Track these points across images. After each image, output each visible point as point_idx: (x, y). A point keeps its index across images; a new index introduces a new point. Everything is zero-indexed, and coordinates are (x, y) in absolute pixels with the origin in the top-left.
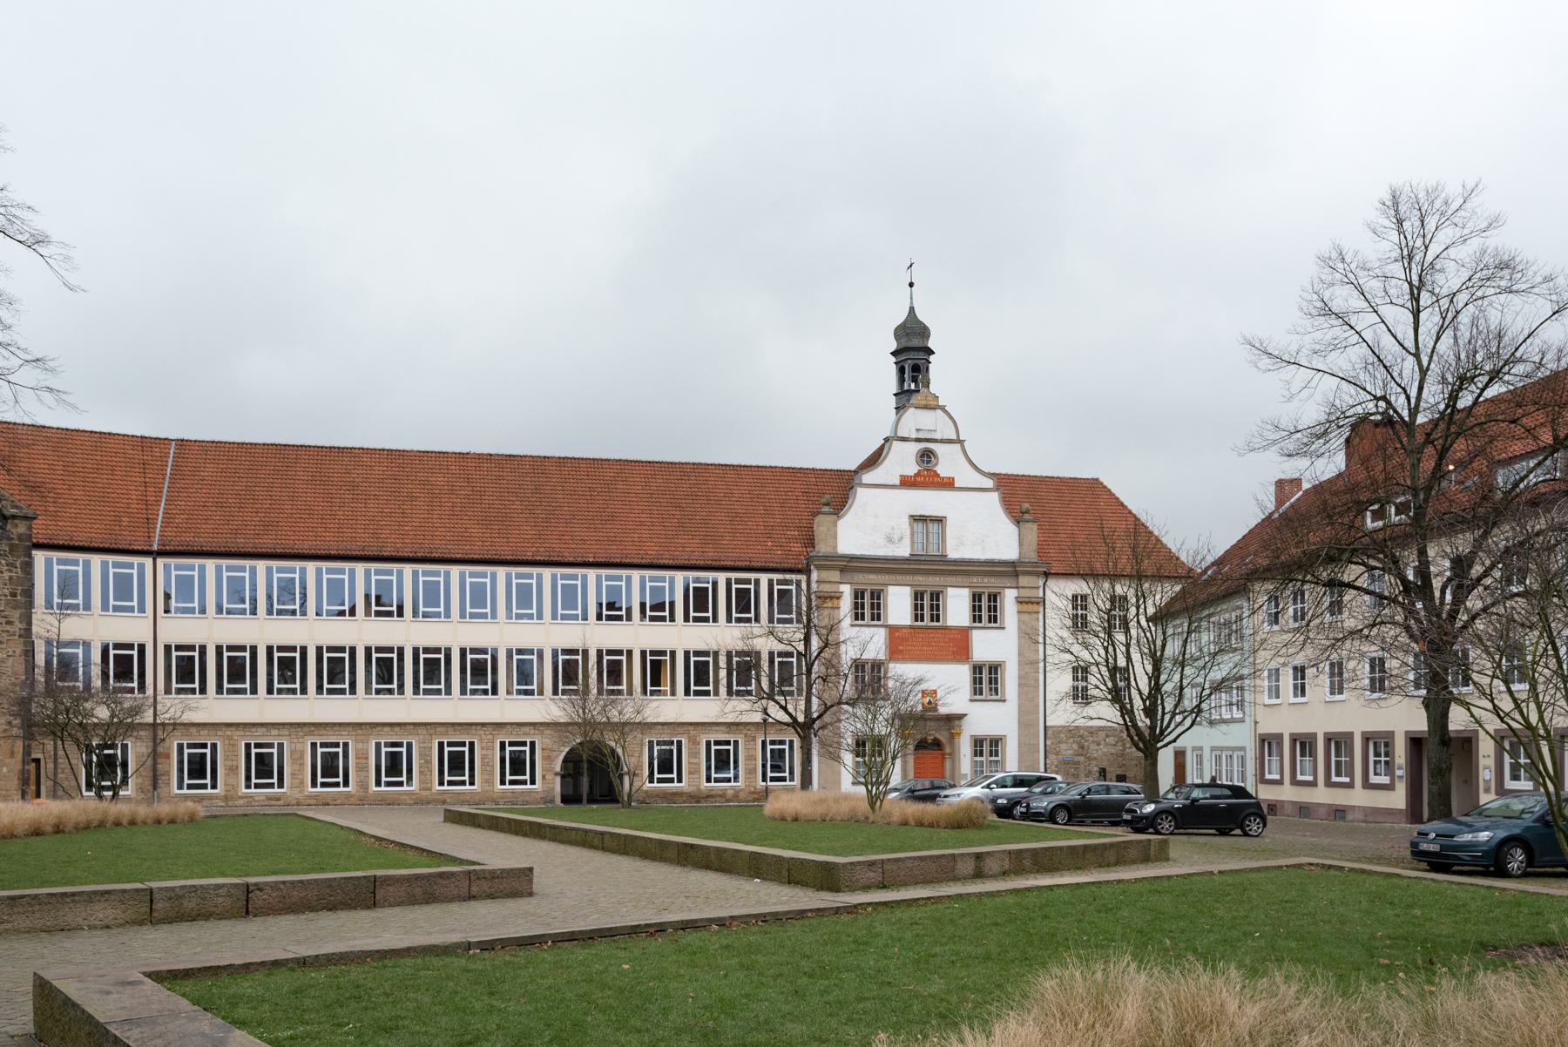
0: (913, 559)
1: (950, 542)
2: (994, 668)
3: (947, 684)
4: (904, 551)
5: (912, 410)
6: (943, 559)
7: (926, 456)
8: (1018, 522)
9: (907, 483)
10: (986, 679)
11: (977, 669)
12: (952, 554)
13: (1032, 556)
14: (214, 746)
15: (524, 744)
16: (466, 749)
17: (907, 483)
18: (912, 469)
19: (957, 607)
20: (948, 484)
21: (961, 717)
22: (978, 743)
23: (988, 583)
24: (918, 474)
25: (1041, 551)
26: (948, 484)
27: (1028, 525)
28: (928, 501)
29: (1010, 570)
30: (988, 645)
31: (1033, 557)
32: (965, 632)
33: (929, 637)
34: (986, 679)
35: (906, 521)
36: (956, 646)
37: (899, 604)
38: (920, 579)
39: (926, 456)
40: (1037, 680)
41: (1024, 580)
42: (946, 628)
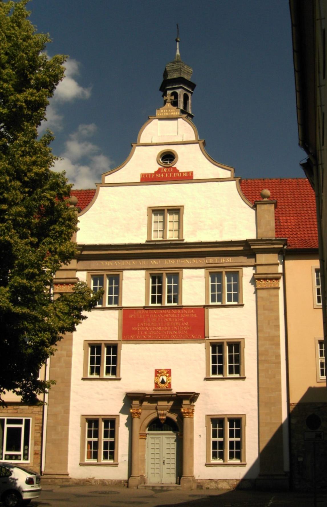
0: (150, 245)
1: (186, 228)
2: (236, 346)
3: (185, 364)
4: (140, 237)
5: (155, 121)
6: (180, 244)
7: (168, 157)
8: (254, 207)
9: (147, 179)
10: (226, 359)
11: (217, 347)
12: (188, 238)
13: (271, 234)
14: (27, 422)
15: (20, 422)
16: (23, 426)
17: (147, 179)
18: (153, 166)
19: (194, 286)
20: (188, 178)
21: (193, 397)
22: (217, 422)
23: (221, 257)
24: (159, 171)
25: (278, 228)
26: (188, 178)
27: (266, 207)
28: (166, 194)
29: (247, 249)
30: (222, 324)
31: (271, 234)
32: (200, 312)
33: (165, 320)
34: (226, 359)
35: (145, 211)
36: (191, 325)
37: (135, 287)
38: (155, 263)
39: (168, 157)
40: (278, 356)
41: (261, 258)
42: (181, 307)
